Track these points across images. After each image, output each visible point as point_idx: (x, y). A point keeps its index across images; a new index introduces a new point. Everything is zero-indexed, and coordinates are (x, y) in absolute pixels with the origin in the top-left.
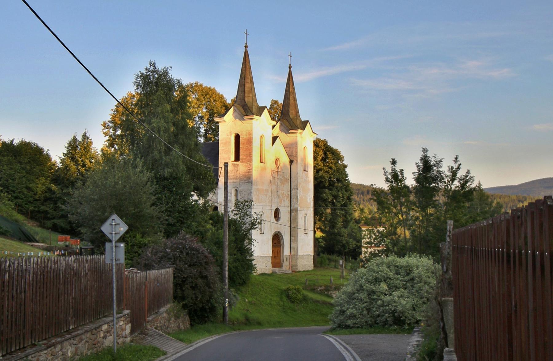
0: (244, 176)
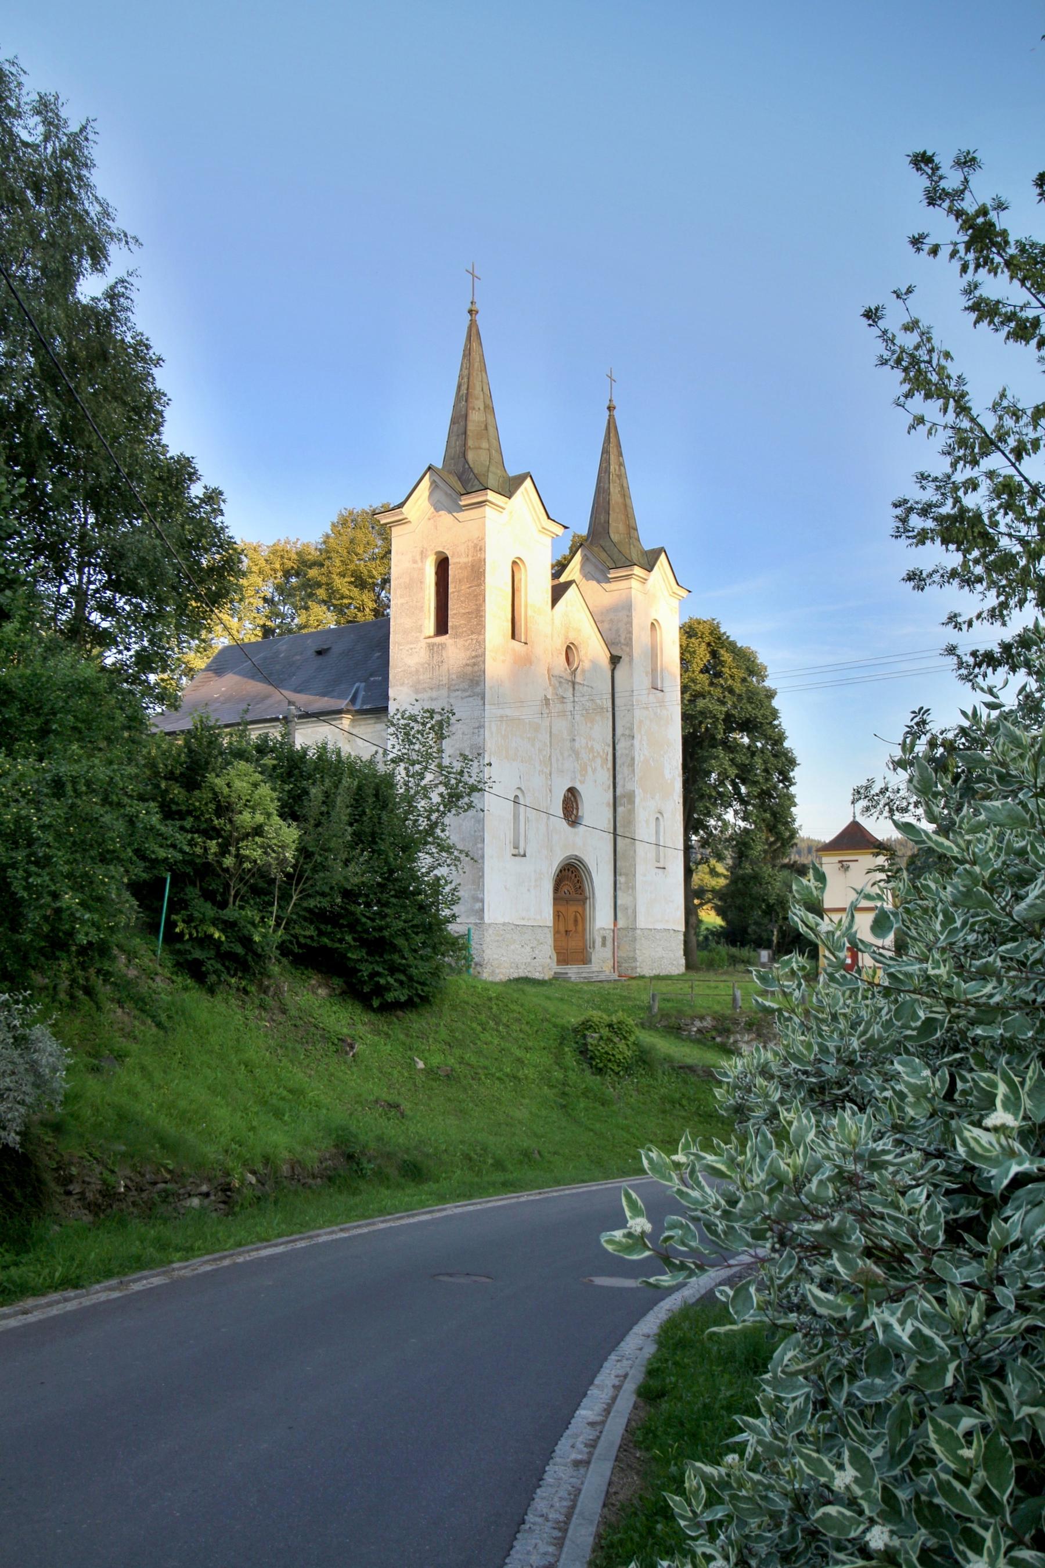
0: (462, 676)
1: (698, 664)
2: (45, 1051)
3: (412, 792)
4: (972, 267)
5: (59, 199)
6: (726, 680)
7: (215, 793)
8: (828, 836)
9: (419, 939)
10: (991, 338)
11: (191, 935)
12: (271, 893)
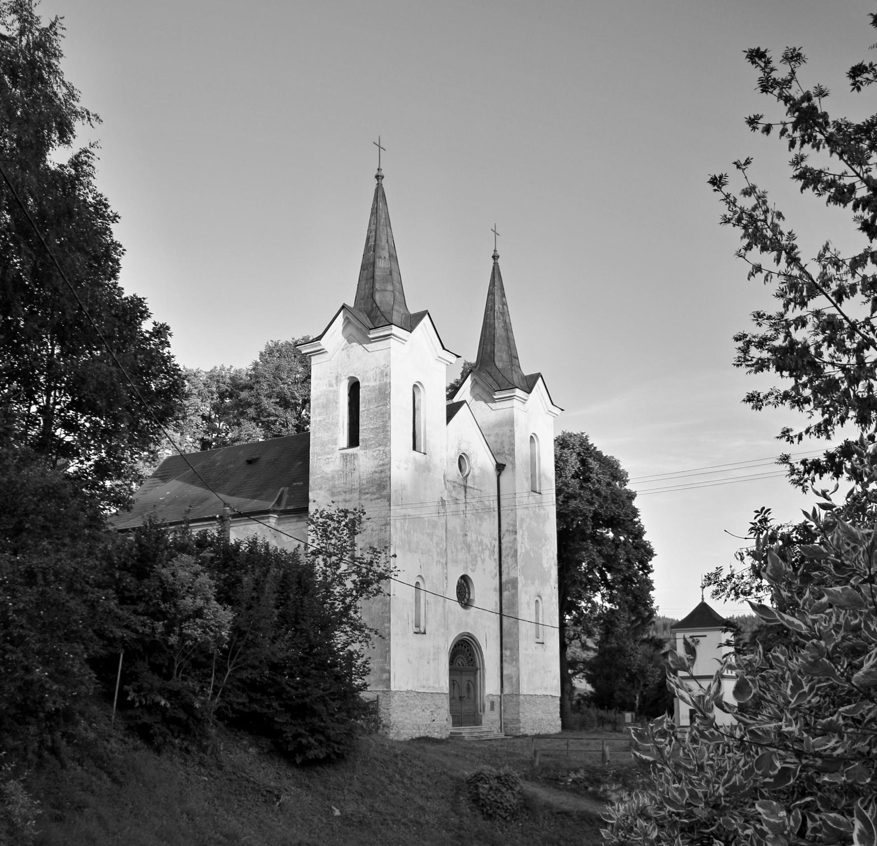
0: (371, 482)
1: (570, 471)
2: (17, 803)
3: (329, 580)
4: (798, 143)
5: (33, 83)
6: (594, 484)
7: (162, 582)
8: (680, 615)
9: (335, 705)
10: (815, 201)
11: (140, 702)
12: (210, 666)
